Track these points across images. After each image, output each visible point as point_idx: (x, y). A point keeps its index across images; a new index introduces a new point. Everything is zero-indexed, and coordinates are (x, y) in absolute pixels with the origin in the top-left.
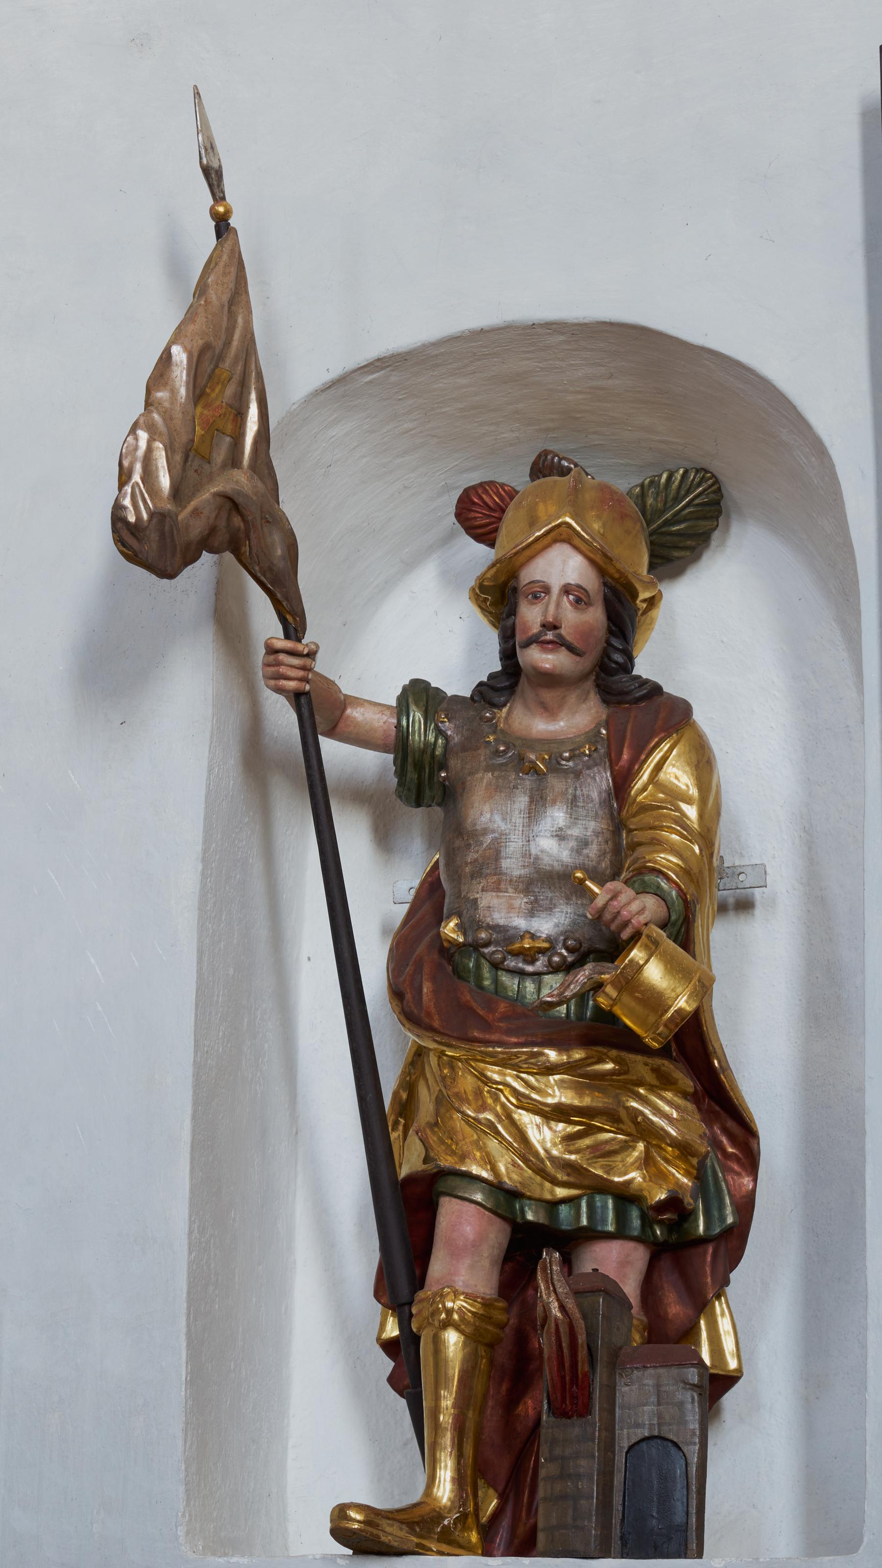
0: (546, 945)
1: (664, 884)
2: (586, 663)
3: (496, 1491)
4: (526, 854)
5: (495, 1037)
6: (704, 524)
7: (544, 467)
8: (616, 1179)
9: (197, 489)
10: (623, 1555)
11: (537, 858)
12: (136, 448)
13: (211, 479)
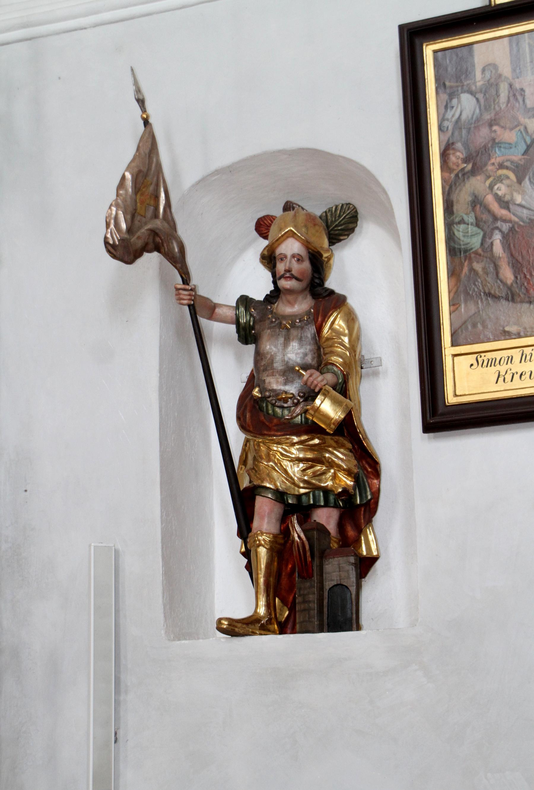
0: (291, 396)
1: (335, 369)
2: (304, 284)
3: (287, 607)
4: (283, 361)
5: (272, 433)
6: (351, 226)
7: (288, 207)
8: (322, 485)
9: (140, 228)
10: (329, 631)
11: (287, 362)
12: (111, 214)
13: (146, 224)
